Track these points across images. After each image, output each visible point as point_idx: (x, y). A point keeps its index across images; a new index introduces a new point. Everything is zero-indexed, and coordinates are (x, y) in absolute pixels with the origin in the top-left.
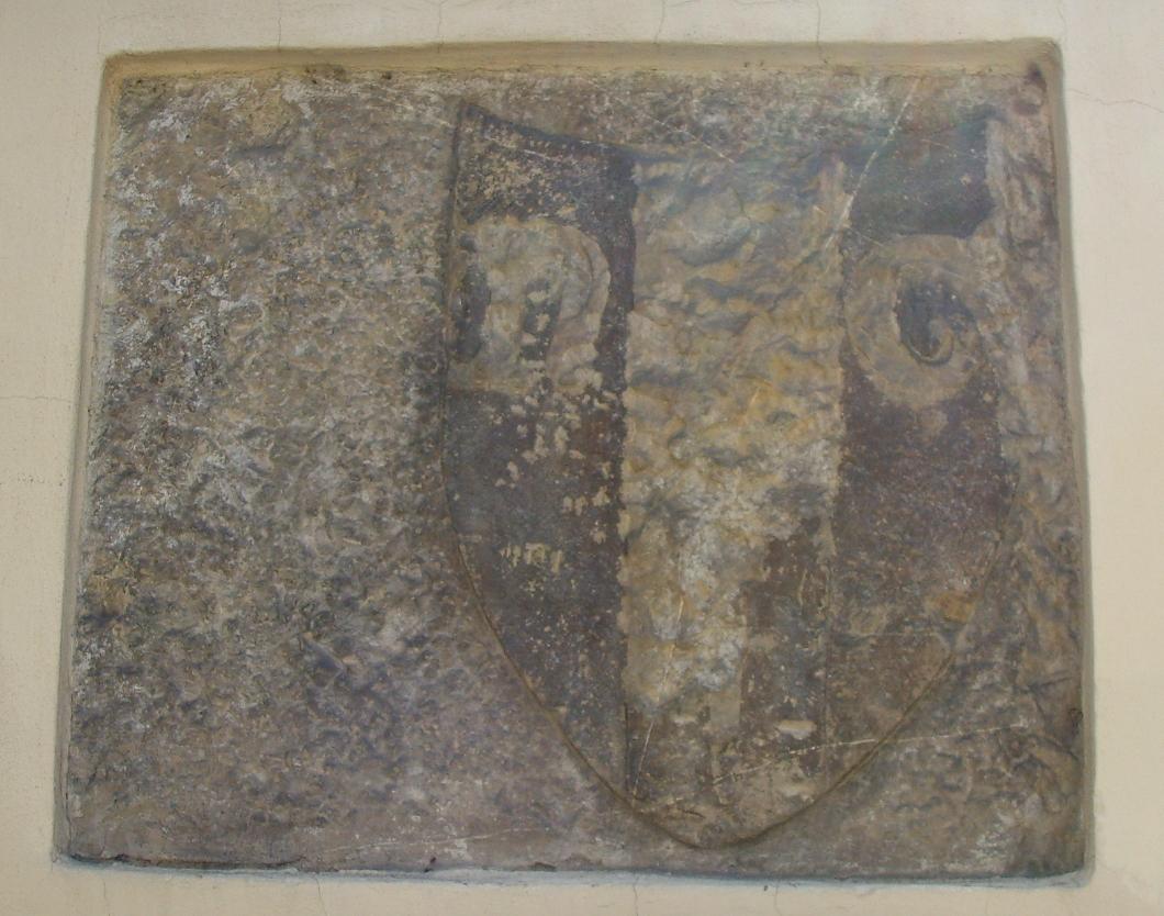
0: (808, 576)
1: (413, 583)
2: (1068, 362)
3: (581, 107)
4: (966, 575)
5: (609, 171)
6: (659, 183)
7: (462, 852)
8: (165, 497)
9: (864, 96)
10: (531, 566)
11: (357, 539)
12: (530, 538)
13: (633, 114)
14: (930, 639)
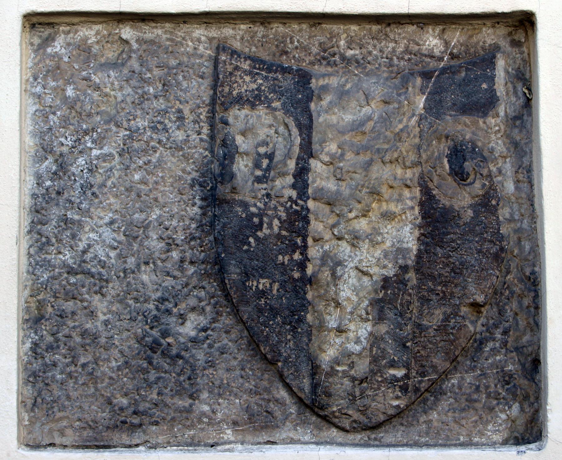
0: (403, 295)
1: (200, 300)
2: (535, 182)
4: (482, 293)
5: (298, 82)
6: (325, 89)
7: (229, 436)
8: (68, 257)
9: (431, 39)
10: (263, 290)
11: (171, 277)
13: (310, 49)
14: (465, 325)
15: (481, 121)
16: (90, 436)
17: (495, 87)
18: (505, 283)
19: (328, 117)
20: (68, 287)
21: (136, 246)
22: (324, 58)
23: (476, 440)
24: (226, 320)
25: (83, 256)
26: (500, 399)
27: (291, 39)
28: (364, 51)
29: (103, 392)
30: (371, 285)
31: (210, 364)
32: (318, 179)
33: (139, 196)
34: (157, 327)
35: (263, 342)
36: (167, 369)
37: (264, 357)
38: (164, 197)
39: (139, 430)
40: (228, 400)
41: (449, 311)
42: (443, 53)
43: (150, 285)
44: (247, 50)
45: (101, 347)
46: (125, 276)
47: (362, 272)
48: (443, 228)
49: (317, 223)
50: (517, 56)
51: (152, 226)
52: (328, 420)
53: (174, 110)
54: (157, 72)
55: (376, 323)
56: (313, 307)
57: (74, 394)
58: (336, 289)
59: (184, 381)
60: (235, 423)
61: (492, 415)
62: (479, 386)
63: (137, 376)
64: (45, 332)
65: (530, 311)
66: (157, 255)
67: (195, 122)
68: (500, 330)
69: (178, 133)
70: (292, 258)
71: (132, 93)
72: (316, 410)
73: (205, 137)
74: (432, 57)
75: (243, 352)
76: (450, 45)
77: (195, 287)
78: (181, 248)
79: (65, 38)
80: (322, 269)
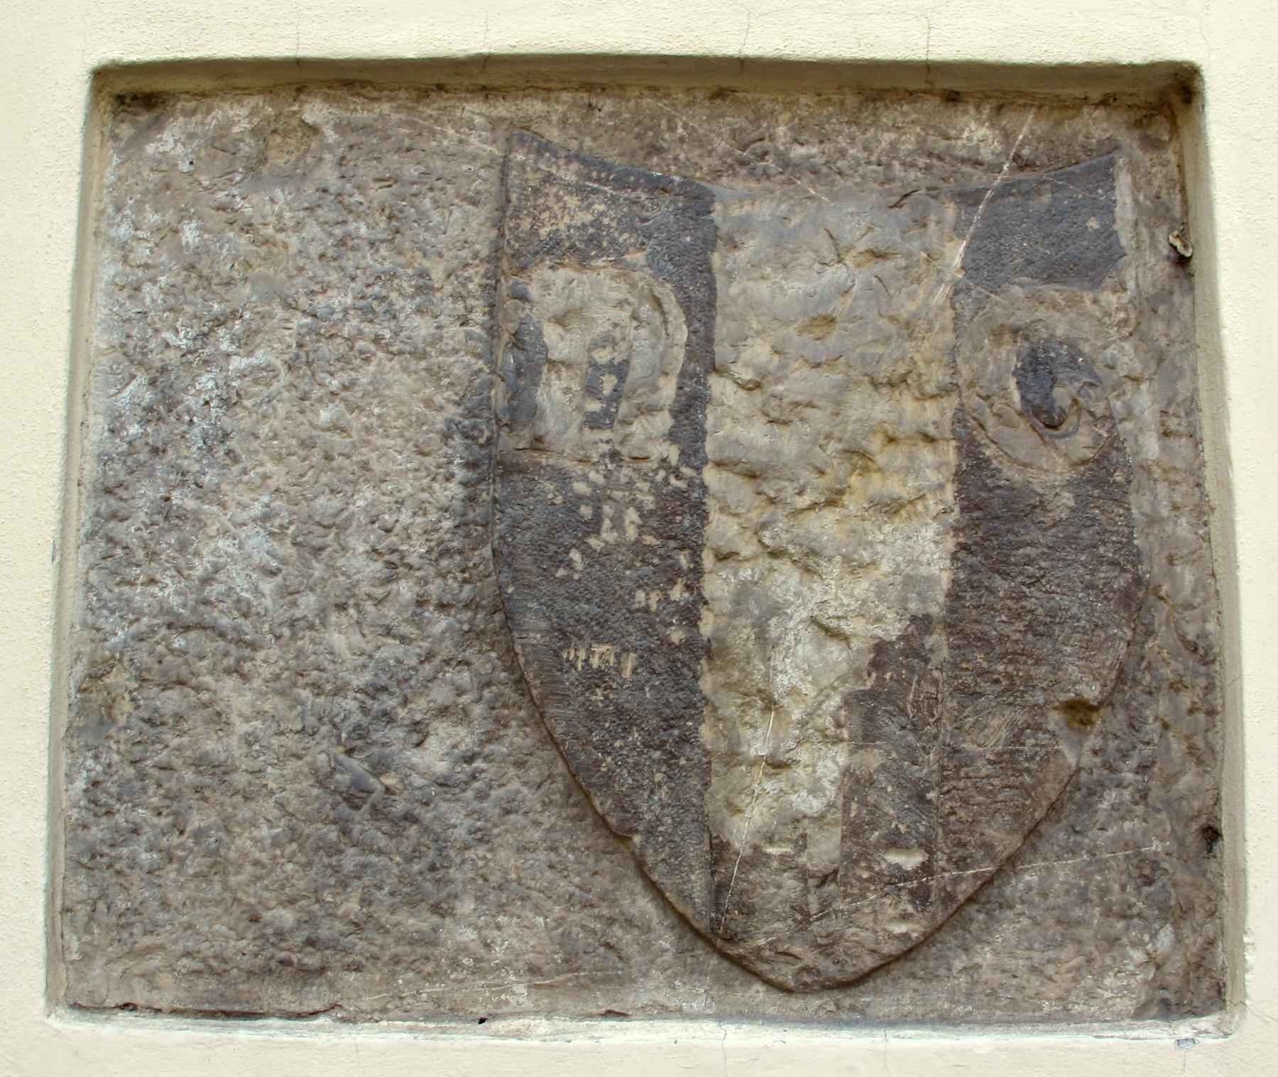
0: (918, 682)
1: (460, 692)
2: (1207, 434)
3: (650, 134)
4: (1096, 679)
5: (684, 209)
6: (746, 225)
7: (521, 1000)
8: (170, 592)
9: (973, 126)
10: (599, 670)
11: (394, 637)
12: (597, 639)
13: (710, 142)
14: (1057, 751)
15: (1087, 298)
16: (213, 991)
17: (1116, 227)
18: (1142, 658)
19: (751, 284)
20: (169, 658)
21: (318, 570)
22: (743, 163)
23: (1078, 1008)
24: (517, 738)
25: (203, 590)
26: (1132, 917)
27: (669, 121)
28: (827, 146)
29: (240, 895)
30: (848, 660)
31: (479, 835)
32: (728, 420)
33: (328, 458)
34: (361, 750)
35: (600, 787)
36: (381, 844)
37: (601, 821)
38: (383, 460)
39: (318, 981)
40: (519, 917)
41: (1021, 718)
42: (999, 155)
43: (347, 655)
44: (574, 144)
45: (237, 792)
46: (294, 637)
47: (827, 630)
48: (1009, 531)
49: (724, 518)
50: (1154, 170)
51: (355, 524)
52: (747, 968)
53: (410, 271)
54: (378, 193)
55: (859, 747)
56: (715, 709)
57: (176, 897)
58: (768, 667)
59: (421, 873)
60: (534, 970)
61: (1115, 953)
62: (1086, 888)
63: (316, 858)
64: (116, 758)
65: (1197, 720)
66: (364, 588)
67: (457, 297)
68: (1133, 762)
69: (417, 320)
70: (667, 597)
71: (321, 235)
72: (719, 942)
73: (477, 330)
74: (977, 163)
75: (555, 810)
76: (1016, 138)
77: (447, 662)
78: (418, 574)
79: (186, 123)
80: (735, 622)
